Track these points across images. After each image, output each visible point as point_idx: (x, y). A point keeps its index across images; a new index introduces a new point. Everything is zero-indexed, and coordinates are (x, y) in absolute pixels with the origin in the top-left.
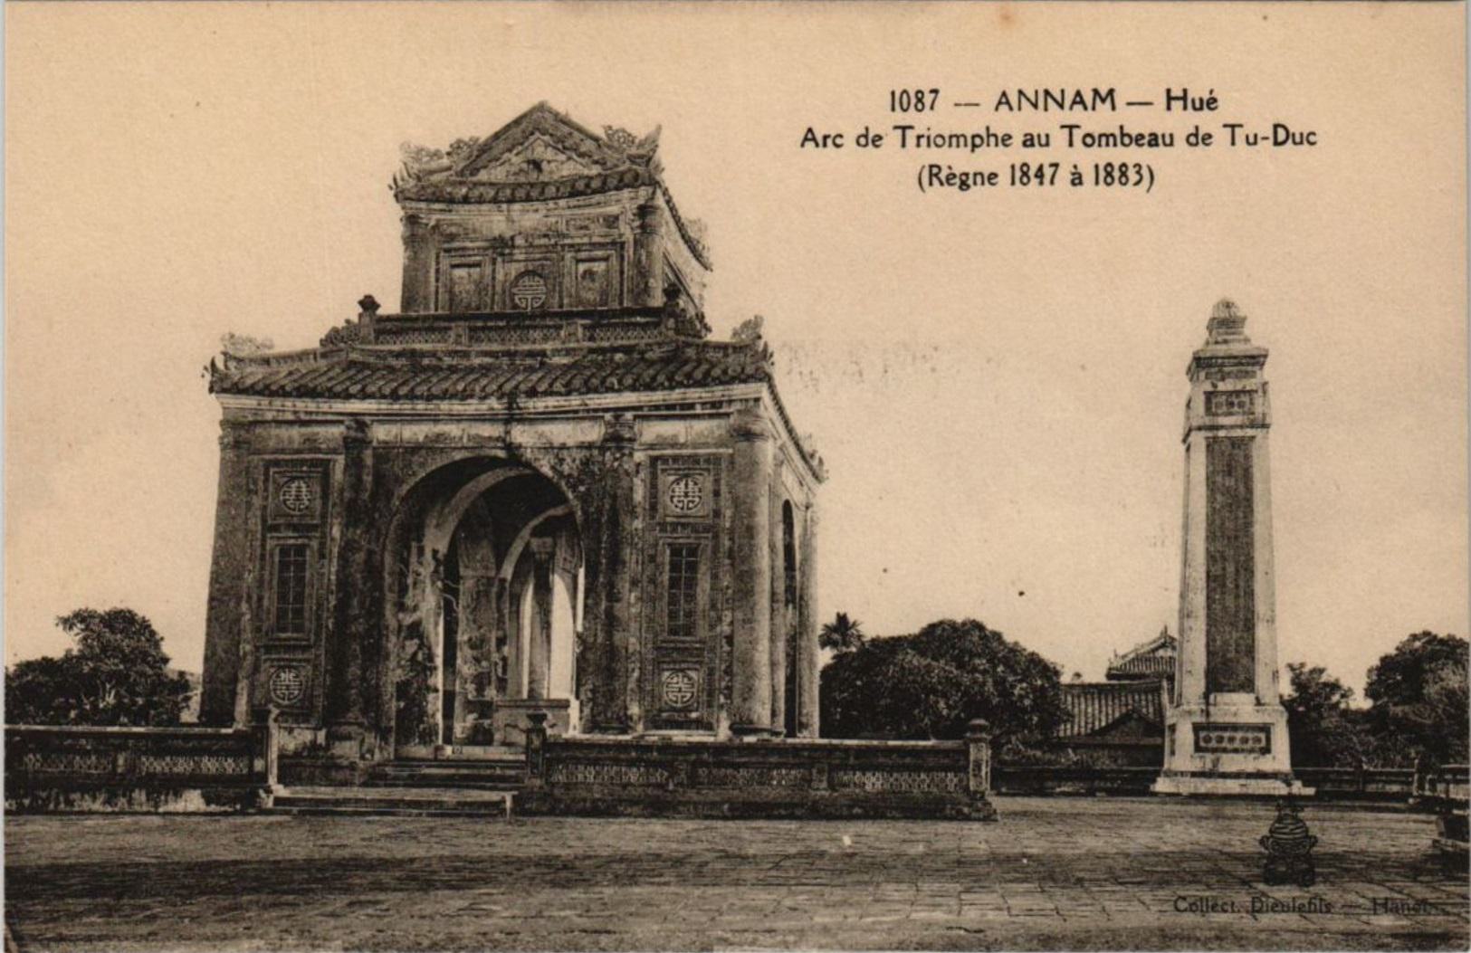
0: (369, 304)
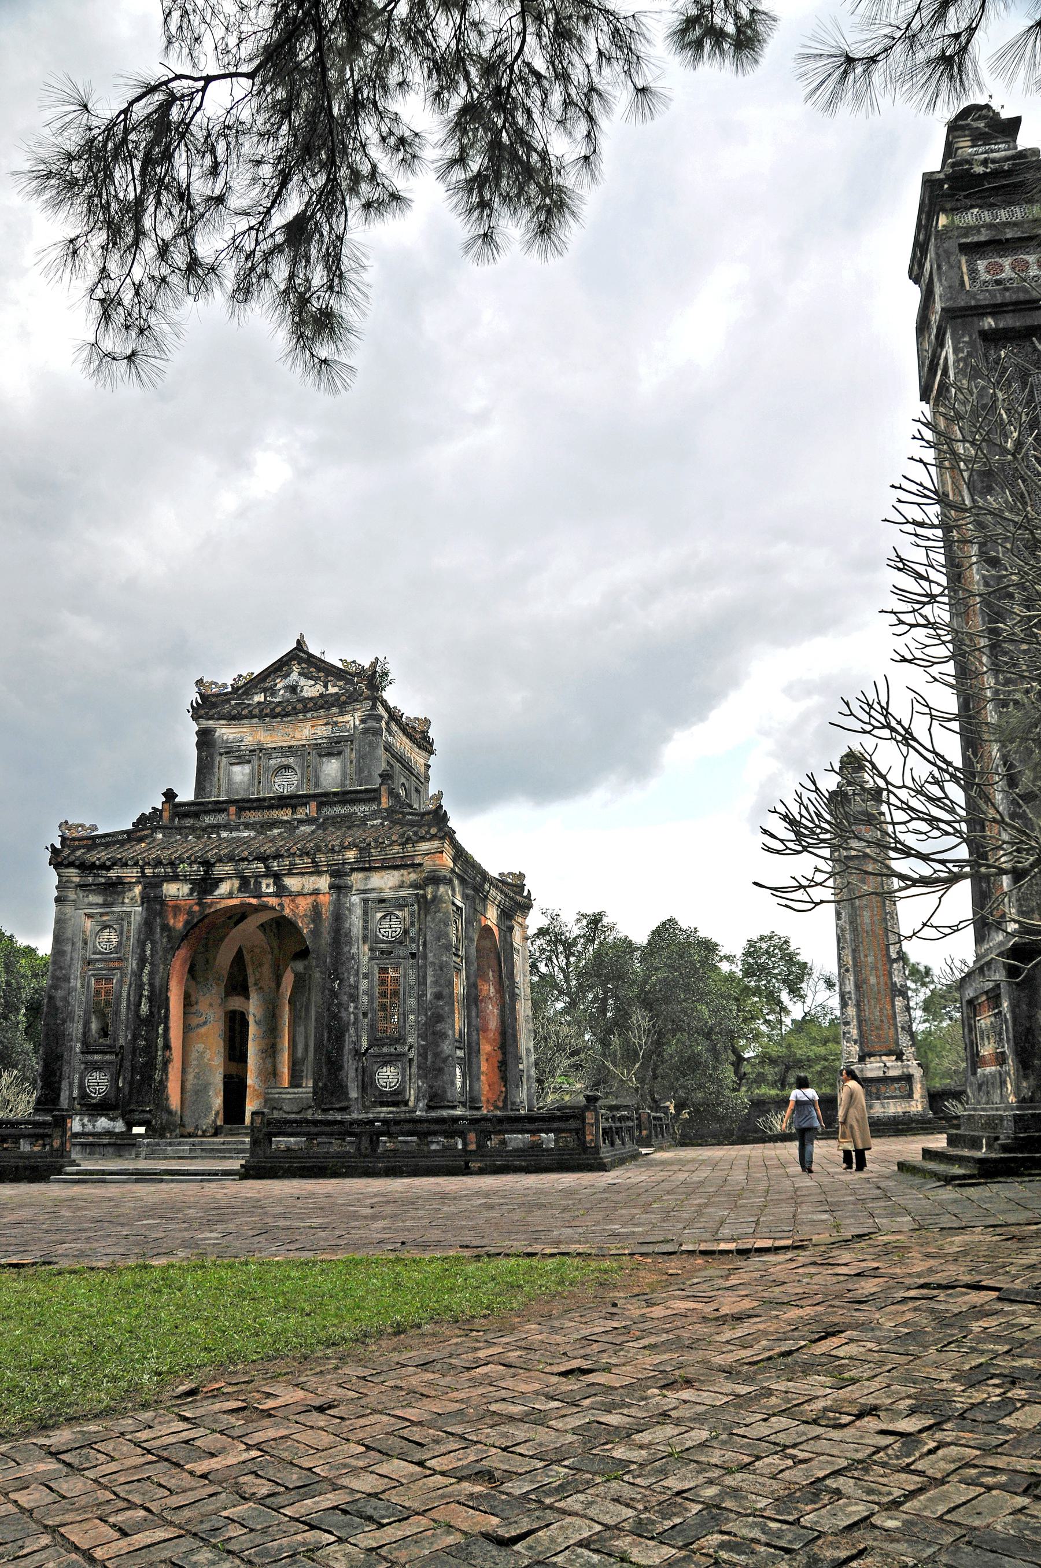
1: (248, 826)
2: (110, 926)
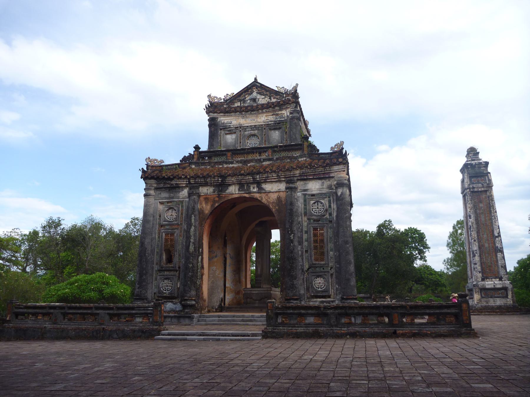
0: (197, 148)
1: (237, 162)
2: (172, 208)
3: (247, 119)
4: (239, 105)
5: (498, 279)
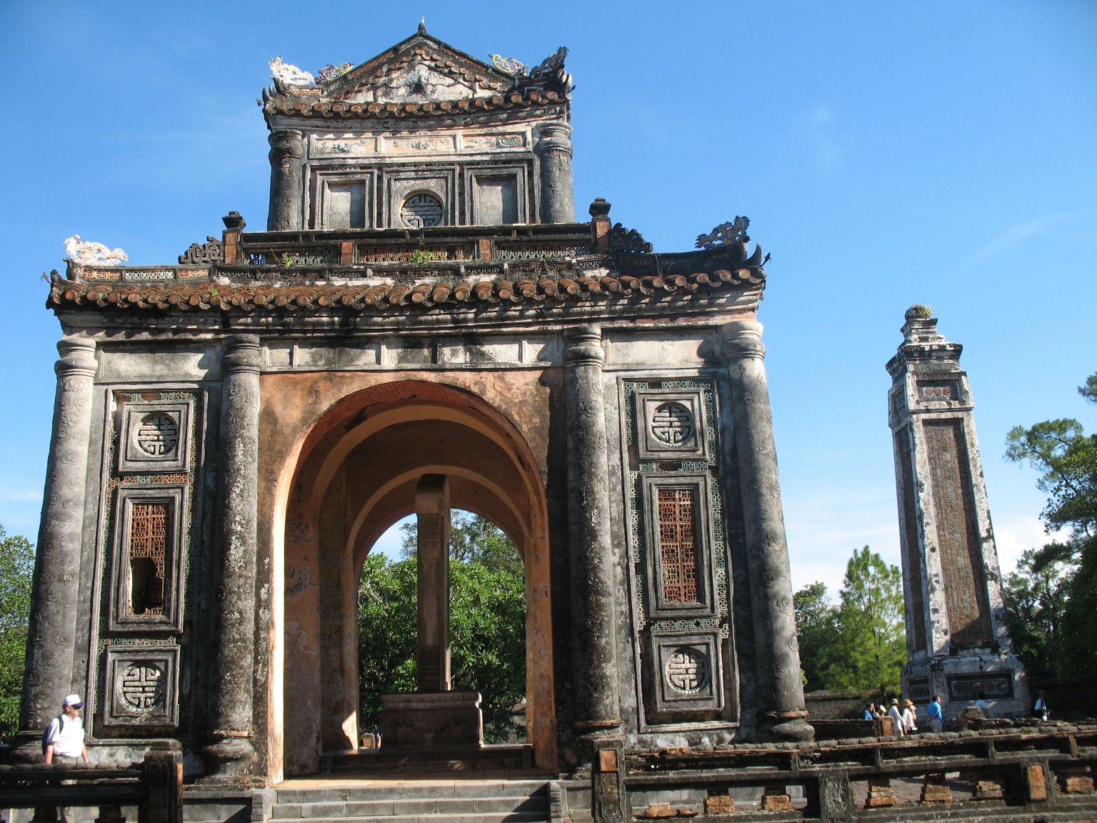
0: (233, 222)
1: (379, 272)
3: (402, 143)
4: (371, 99)
5: (988, 650)
